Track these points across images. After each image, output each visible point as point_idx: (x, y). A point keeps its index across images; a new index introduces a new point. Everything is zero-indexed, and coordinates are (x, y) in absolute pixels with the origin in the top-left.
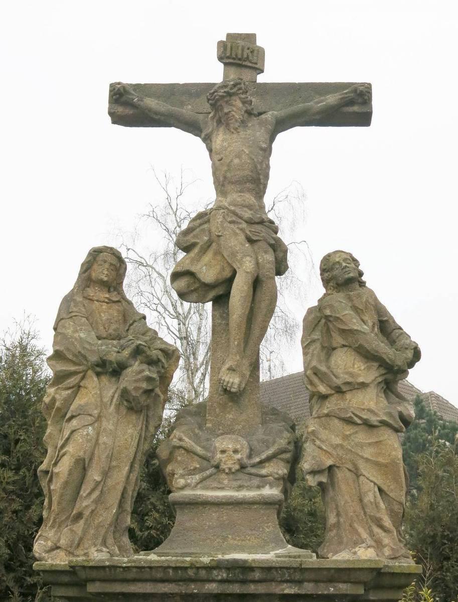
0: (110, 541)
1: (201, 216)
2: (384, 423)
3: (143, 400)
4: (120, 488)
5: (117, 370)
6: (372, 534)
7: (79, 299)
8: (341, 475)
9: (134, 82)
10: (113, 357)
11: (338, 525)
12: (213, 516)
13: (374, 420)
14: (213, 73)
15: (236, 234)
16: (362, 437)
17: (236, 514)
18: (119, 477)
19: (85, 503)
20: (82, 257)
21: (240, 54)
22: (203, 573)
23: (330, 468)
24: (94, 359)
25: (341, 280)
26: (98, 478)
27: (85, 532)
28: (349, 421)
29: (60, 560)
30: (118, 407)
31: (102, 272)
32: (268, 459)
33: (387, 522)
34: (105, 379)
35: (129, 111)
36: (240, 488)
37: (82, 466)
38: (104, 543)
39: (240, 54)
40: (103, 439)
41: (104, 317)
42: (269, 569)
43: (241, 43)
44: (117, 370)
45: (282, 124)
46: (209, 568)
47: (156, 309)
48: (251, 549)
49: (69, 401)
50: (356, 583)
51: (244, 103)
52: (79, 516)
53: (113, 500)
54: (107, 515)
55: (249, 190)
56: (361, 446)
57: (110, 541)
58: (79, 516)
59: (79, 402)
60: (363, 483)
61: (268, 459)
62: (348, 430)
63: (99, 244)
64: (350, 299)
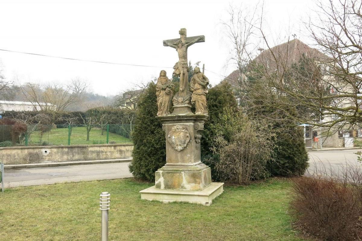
0: (167, 113)
1: (177, 63)
2: (202, 94)
3: (169, 93)
4: (167, 106)
5: (165, 89)
6: (201, 110)
7: (160, 79)
8: (196, 102)
9: (167, 40)
10: (164, 88)
11: (197, 109)
12: (178, 109)
13: (200, 94)
14: (178, 36)
15: (180, 67)
16: (199, 96)
17: (182, 108)
18: (167, 104)
19: (162, 108)
20: (160, 72)
21: (183, 32)
22: (175, 117)
23: (195, 101)
24: (161, 88)
25: (196, 72)
26: (163, 105)
27: (163, 112)
28: (196, 94)
29: (160, 116)
30: (165, 95)
31: (162, 74)
32: (186, 100)
33: (203, 108)
34: (163, 91)
35: (166, 45)
36: (182, 105)
37: (161, 103)
38: (166, 113)
39: (183, 32)
40: (164, 99)
41: (163, 81)
42: (182, 116)
43: (183, 30)
44: (165, 89)
45: (188, 46)
46: (175, 116)
47: (355, 12)
48: (183, 113)
49: (159, 94)
50: (194, 117)
51: (181, 44)
52: (161, 110)
53: (166, 107)
54: (165, 110)
55: (183, 58)
56: (199, 98)
57: (167, 113)
58: (161, 110)
59: (160, 94)
60: (277, 76)
61: (186, 100)
62: (197, 96)
63: (162, 70)
64: (197, 75)
